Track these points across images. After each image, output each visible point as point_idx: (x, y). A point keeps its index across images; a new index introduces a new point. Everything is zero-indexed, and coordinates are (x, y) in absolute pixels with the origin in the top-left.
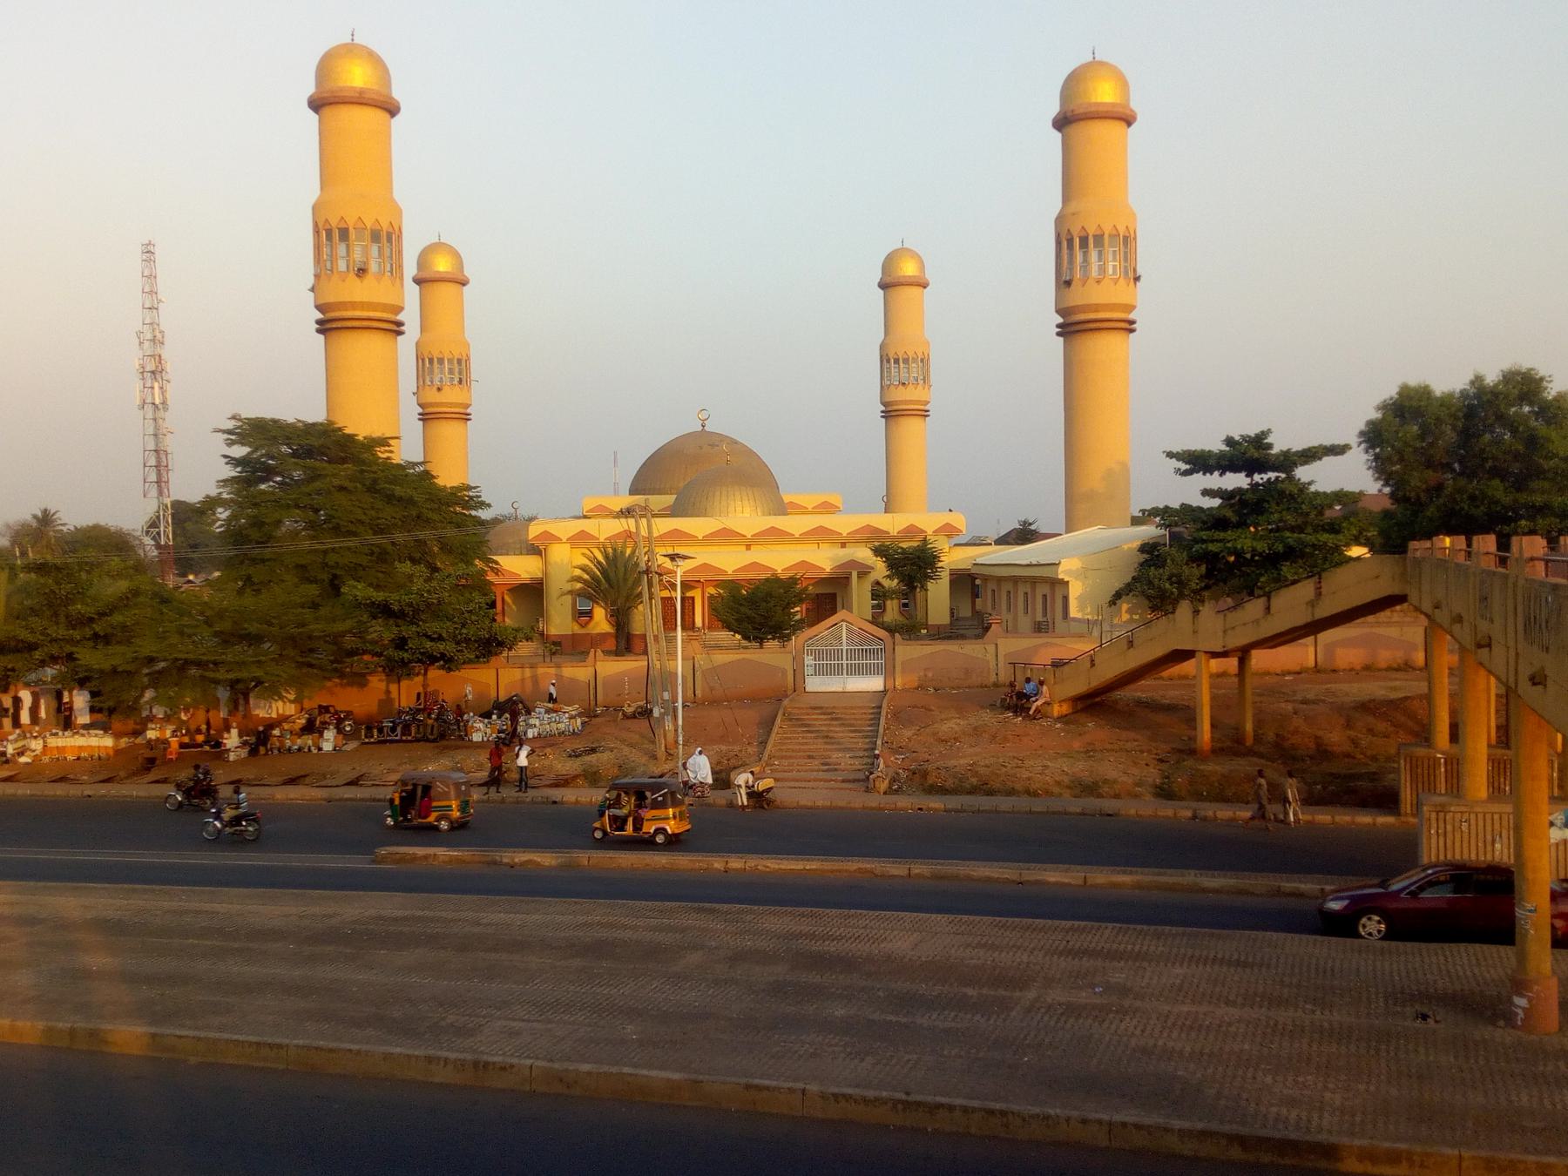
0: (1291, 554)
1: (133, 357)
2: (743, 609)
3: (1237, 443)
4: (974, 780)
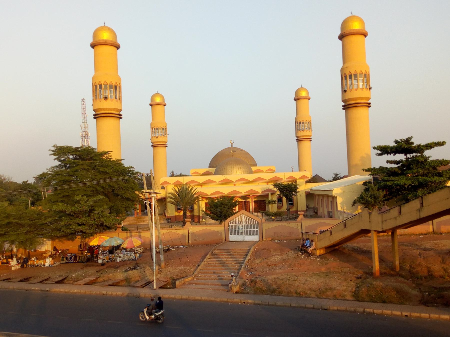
0: (422, 185)
1: (80, 133)
2: (213, 209)
3: (399, 142)
4: (275, 286)
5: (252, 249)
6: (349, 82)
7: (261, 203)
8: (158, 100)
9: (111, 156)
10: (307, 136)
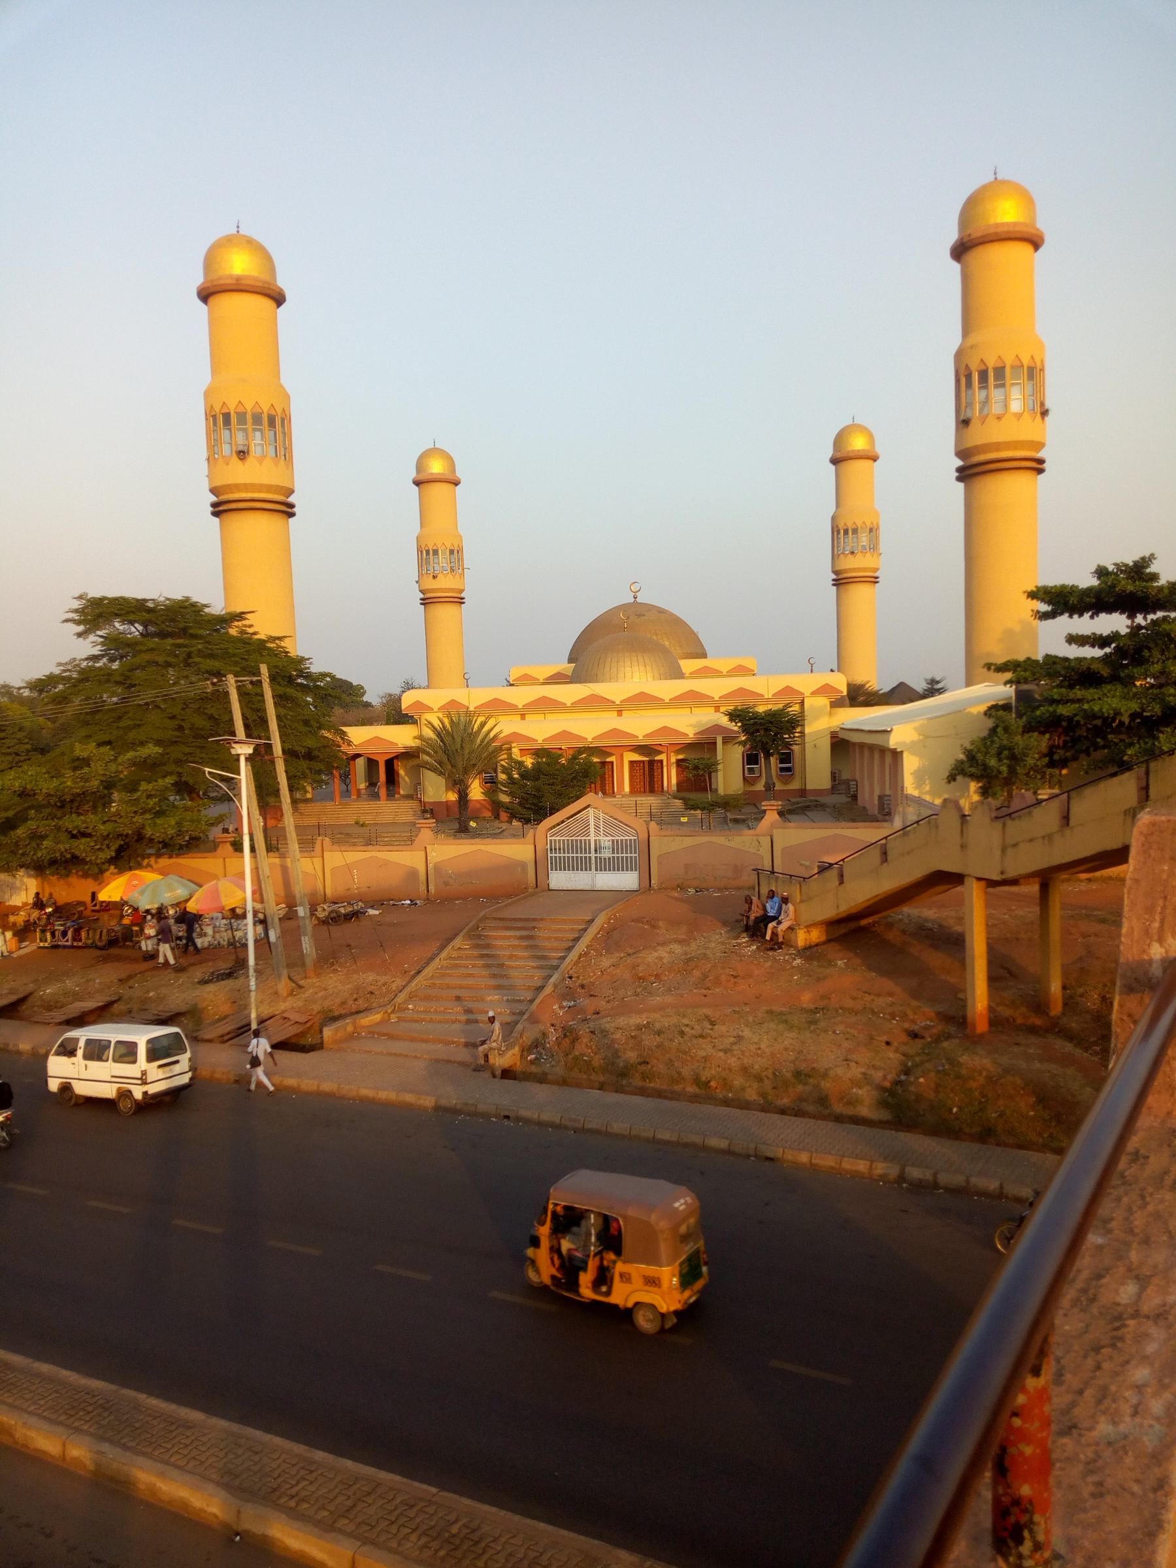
4: (632, 1056)
5: (600, 921)
6: (979, 395)
7: (697, 762)
8: (436, 467)
9: (251, 626)
10: (864, 569)
